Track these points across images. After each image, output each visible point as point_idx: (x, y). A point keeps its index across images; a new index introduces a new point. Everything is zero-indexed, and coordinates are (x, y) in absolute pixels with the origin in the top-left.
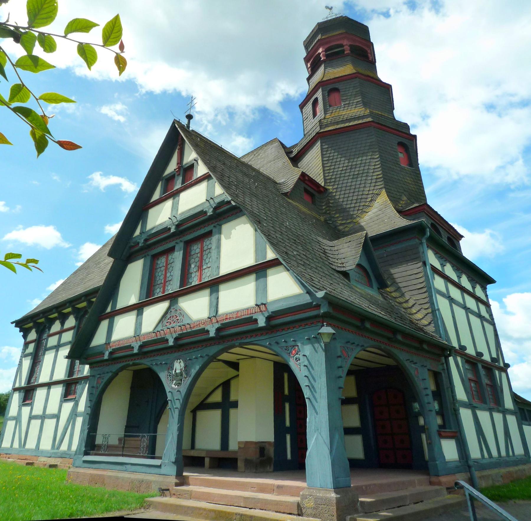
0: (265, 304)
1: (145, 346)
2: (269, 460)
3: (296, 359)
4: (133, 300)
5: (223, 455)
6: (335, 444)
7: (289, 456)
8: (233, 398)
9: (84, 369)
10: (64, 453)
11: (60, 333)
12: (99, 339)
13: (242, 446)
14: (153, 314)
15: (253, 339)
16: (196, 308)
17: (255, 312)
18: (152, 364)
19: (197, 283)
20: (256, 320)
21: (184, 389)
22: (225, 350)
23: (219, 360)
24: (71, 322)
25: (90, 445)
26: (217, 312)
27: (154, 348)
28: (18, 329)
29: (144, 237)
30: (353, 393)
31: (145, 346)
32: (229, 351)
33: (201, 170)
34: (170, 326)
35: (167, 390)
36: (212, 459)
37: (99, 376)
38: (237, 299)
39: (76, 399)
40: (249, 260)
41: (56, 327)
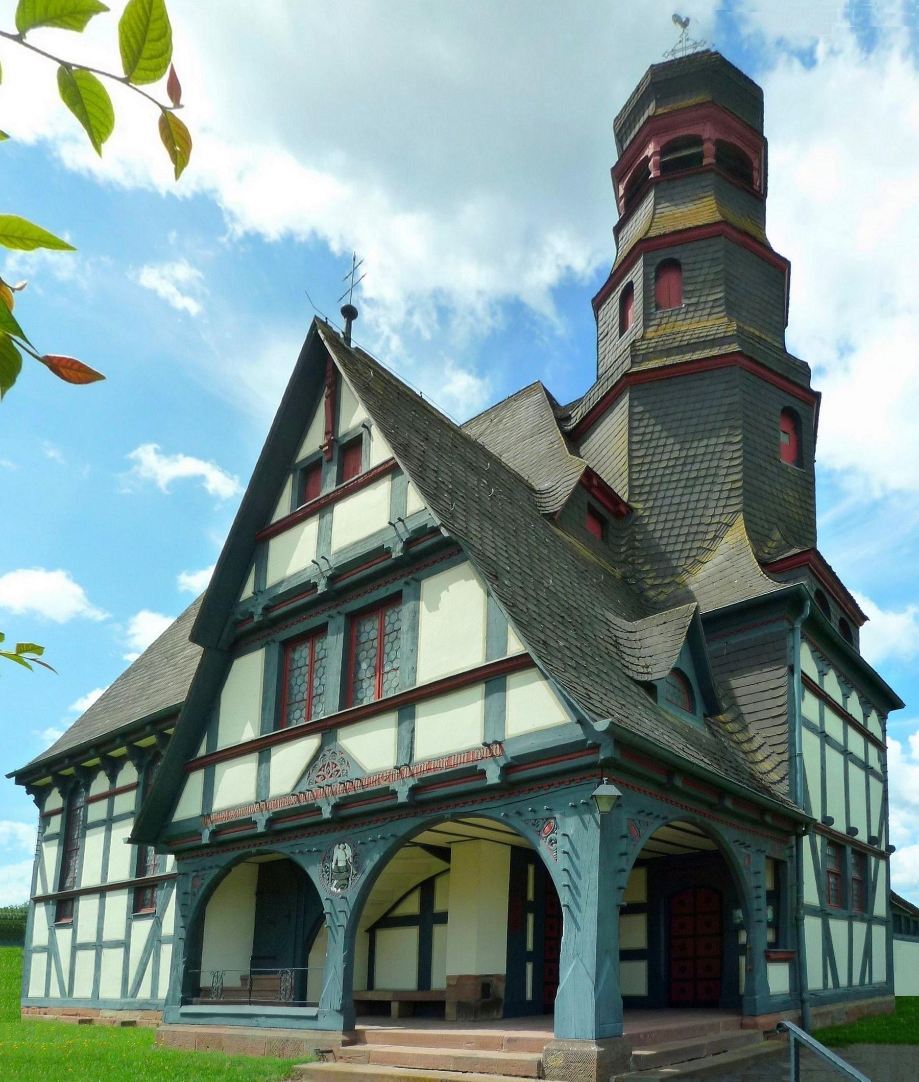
0: (500, 743)
4: (250, 733)
7: (529, 996)
8: (438, 907)
9: (165, 862)
10: (146, 1002)
11: (110, 795)
12: (188, 807)
14: (291, 760)
15: (476, 807)
16: (371, 749)
17: (483, 758)
18: (292, 853)
19: (373, 701)
20: (483, 773)
21: (352, 893)
22: (427, 826)
24: (129, 774)
25: (191, 988)
27: (295, 823)
28: (23, 789)
29: (263, 601)
33: (378, 451)
34: (323, 784)
35: (323, 895)
37: (195, 874)
38: (450, 732)
39: (157, 915)
40: (473, 657)
41: (101, 784)
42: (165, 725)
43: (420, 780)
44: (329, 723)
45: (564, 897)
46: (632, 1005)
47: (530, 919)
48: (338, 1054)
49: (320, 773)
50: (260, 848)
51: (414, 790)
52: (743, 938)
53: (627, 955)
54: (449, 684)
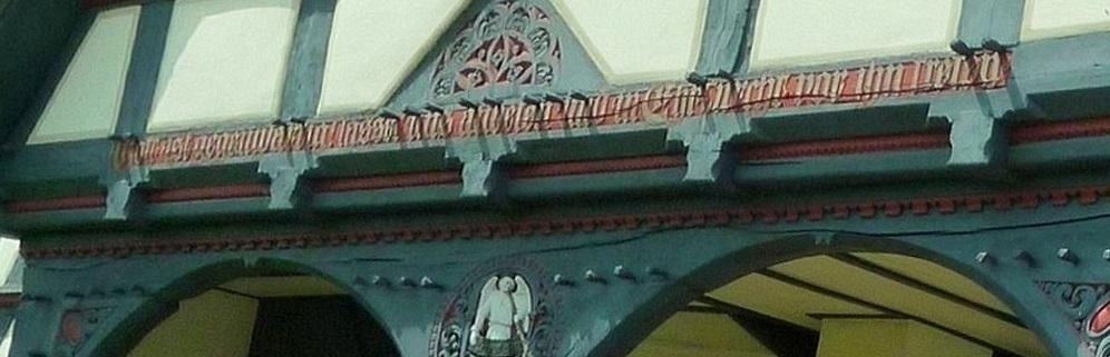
0: (1003, 51)
15: (907, 224)
17: (947, 87)
18: (359, 281)
20: (942, 129)
22: (759, 260)
23: (719, 307)
26: (743, 52)
34: (476, 95)
37: (70, 303)
43: (757, 122)
49: (472, 64)
50: (268, 255)
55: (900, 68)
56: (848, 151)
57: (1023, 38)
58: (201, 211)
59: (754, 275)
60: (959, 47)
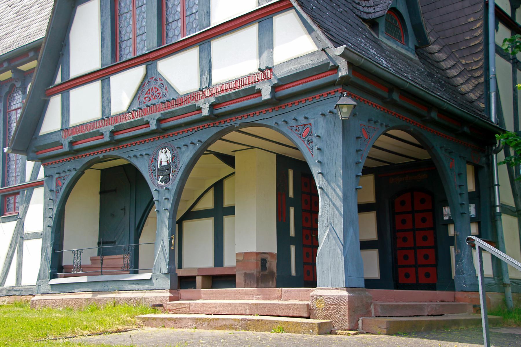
0: (270, 69)
1: (117, 131)
2: (272, 274)
3: (308, 141)
4: (96, 65)
5: (218, 272)
6: (349, 239)
7: (293, 273)
8: (227, 203)
10: (12, 289)
12: (51, 123)
13: (241, 258)
14: (125, 85)
15: (256, 118)
16: (181, 73)
17: (259, 81)
18: (129, 157)
20: (259, 91)
21: (173, 184)
22: (219, 136)
23: (211, 152)
25: (57, 266)
26: (210, 83)
27: (122, 134)
30: (370, 198)
31: (117, 131)
32: (223, 138)
34: (149, 103)
35: (153, 189)
36: (204, 276)
37: (57, 176)
38: (235, 62)
42: (17, 63)
43: (217, 98)
44: (151, 56)
45: (319, 181)
46: (370, 284)
47: (292, 210)
48: (168, 307)
49: (147, 96)
50: (105, 154)
51: (212, 106)
52: (451, 231)
53: (365, 245)
54: (230, 25)
55: (247, 78)
56: (239, 102)
57: (275, 64)
58: (55, 153)
59: (219, 140)
60: (260, 70)
